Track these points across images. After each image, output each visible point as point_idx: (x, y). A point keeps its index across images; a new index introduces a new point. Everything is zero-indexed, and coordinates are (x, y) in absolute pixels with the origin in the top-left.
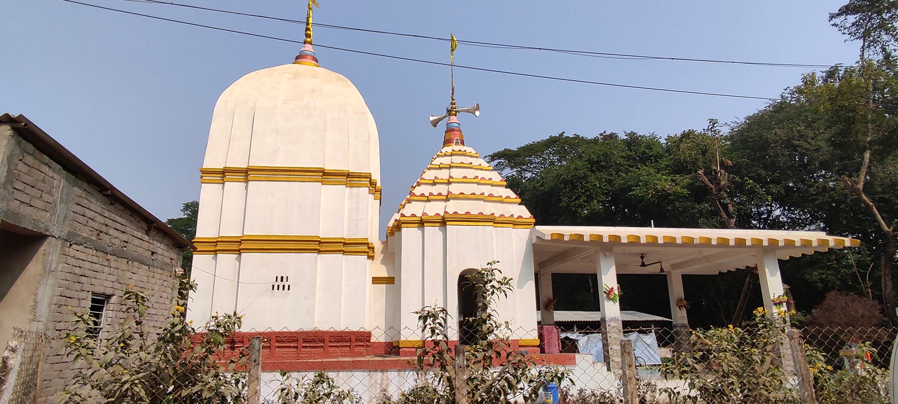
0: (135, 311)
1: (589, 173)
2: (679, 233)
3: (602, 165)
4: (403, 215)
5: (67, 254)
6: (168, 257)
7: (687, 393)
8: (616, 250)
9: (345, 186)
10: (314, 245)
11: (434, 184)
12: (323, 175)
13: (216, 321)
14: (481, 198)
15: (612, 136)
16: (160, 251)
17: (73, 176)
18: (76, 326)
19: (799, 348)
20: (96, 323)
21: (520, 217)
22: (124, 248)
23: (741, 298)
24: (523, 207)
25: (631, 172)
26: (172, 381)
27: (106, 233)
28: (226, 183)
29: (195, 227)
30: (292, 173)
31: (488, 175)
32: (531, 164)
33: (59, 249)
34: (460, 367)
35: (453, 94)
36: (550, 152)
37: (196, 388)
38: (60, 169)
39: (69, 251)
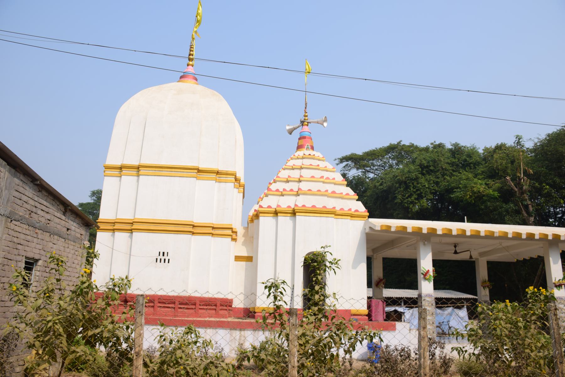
0: (56, 271)
1: (420, 175)
2: (483, 228)
3: (431, 169)
4: (261, 207)
6: (79, 233)
7: (472, 351)
8: (433, 239)
9: (215, 181)
10: (189, 228)
11: (288, 181)
12: (198, 172)
13: (113, 282)
14: (325, 194)
15: (441, 146)
16: (73, 228)
17: (14, 170)
19: (554, 318)
20: (447, 182)
21: (357, 211)
22: (48, 225)
23: (535, 281)
24: (360, 203)
25: (454, 176)
26: (81, 324)
27: (36, 213)
29: (99, 210)
30: (173, 170)
31: (331, 175)
32: (374, 166)
33: (3, 223)
34: (294, 325)
35: (306, 108)
36: (390, 157)
38: (5, 164)
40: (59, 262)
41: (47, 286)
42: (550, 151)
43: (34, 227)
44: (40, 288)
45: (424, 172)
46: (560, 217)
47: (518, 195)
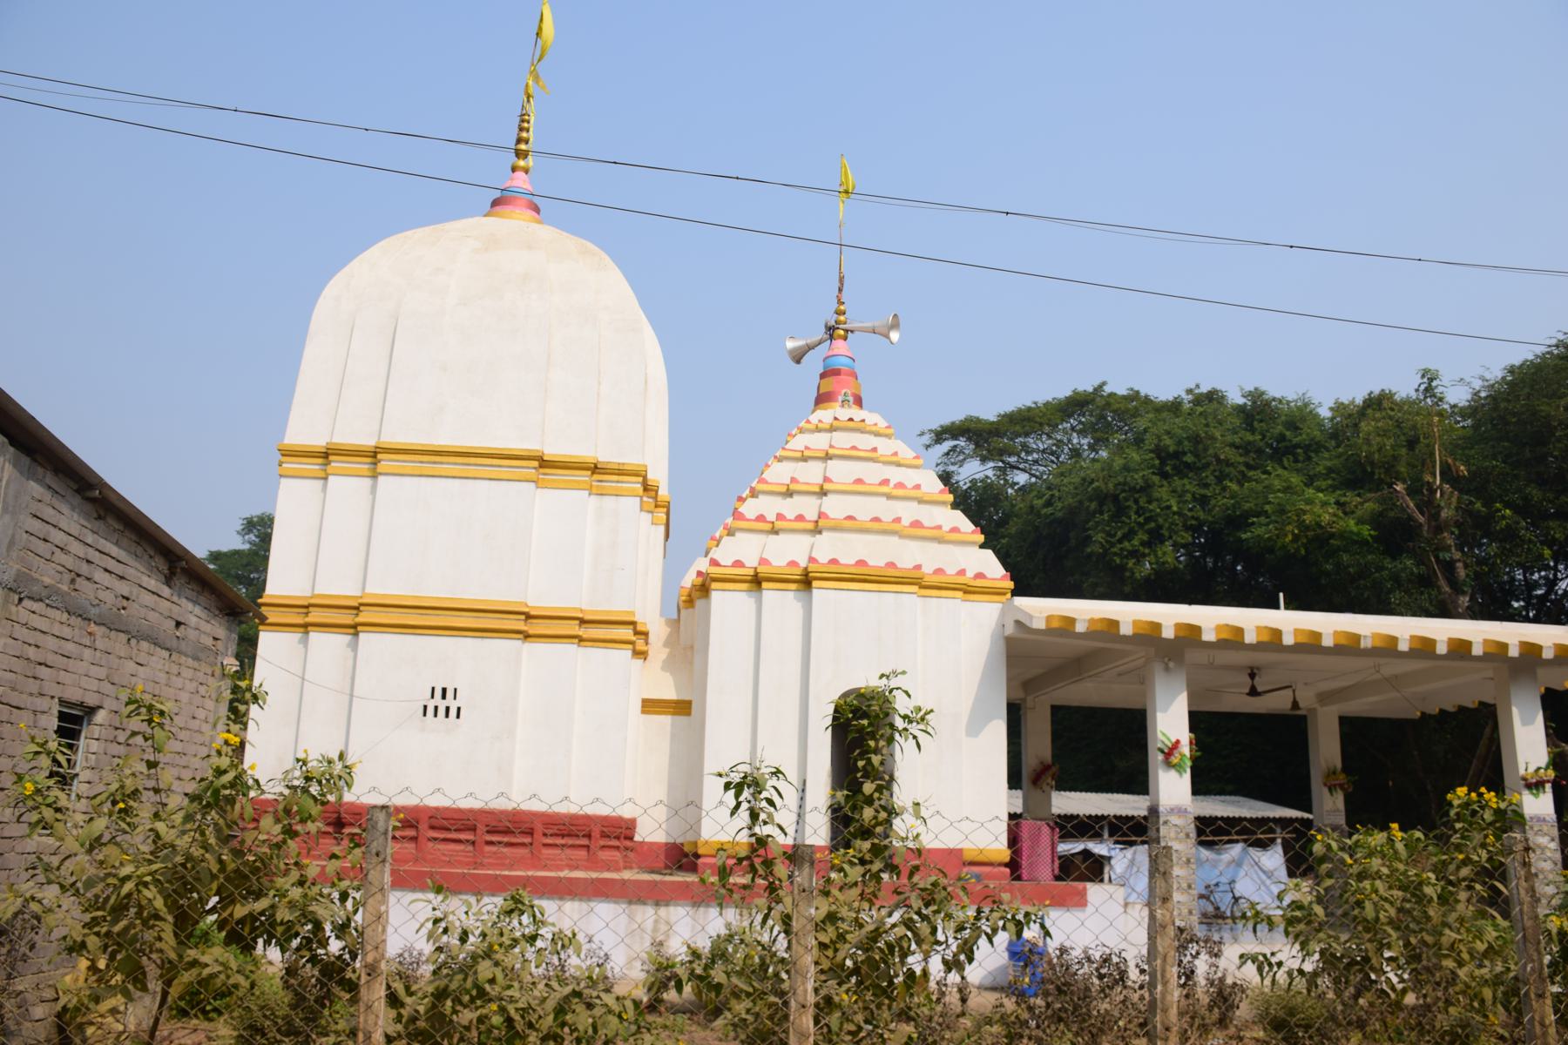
1: (1156, 479)
2: (1329, 625)
4: (714, 563)
5: (14, 619)
6: (209, 635)
7: (1295, 964)
8: (1193, 656)
10: (514, 622)
11: (789, 494)
12: (541, 467)
13: (304, 768)
14: (893, 529)
15: (1213, 397)
16: (193, 620)
18: (33, 764)
19: (1522, 873)
21: (980, 576)
22: (123, 611)
25: (1250, 480)
26: (214, 886)
27: (88, 579)
28: (330, 478)
29: (265, 570)
30: (473, 460)
31: (910, 477)
32: (1028, 453)
34: (804, 891)
35: (840, 290)
36: (1073, 429)
37: (263, 904)
38: (4, 442)
39: (18, 611)
40: (153, 714)
41: (121, 781)
42: (1514, 415)
43: (85, 616)
44: (100, 788)
45: (1168, 468)
46: (1541, 595)
47: (1425, 534)
